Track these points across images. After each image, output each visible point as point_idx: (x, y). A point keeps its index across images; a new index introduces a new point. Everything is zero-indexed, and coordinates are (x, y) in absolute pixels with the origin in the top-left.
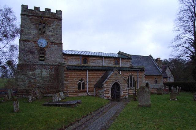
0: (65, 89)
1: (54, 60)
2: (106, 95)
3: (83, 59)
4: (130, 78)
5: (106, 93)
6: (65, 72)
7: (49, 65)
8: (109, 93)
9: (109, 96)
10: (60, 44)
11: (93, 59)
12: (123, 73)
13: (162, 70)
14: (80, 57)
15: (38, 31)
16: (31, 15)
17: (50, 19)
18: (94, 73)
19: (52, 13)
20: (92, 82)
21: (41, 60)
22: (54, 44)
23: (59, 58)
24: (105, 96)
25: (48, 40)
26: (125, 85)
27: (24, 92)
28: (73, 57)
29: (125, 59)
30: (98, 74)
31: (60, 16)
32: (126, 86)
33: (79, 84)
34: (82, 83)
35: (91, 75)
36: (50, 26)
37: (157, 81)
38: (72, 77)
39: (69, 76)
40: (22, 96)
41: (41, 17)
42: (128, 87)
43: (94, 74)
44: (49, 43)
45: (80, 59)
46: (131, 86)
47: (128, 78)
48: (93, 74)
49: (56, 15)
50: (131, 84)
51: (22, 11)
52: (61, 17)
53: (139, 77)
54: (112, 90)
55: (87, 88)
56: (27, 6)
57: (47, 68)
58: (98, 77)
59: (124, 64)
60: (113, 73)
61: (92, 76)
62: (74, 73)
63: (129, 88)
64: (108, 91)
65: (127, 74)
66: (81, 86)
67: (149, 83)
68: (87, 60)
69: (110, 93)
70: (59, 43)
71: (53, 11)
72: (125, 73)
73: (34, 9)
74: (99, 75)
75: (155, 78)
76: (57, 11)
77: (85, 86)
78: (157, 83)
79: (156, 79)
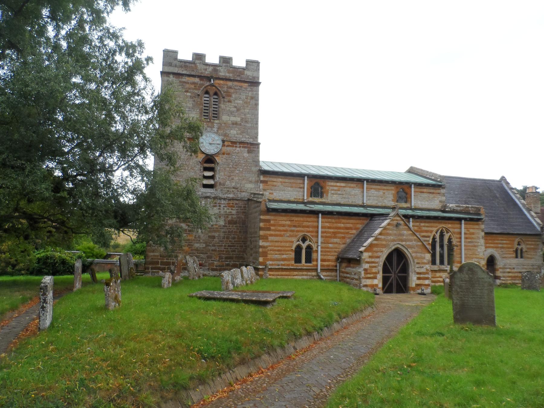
0: (261, 259)
1: (238, 186)
2: (369, 282)
3: (313, 183)
4: (438, 239)
5: (369, 276)
6: (262, 217)
7: (224, 199)
8: (375, 278)
9: (377, 285)
10: (253, 147)
11: (338, 184)
12: (418, 224)
13: (539, 221)
14: (304, 180)
15: (201, 113)
16: (184, 72)
17: (230, 84)
18: (337, 220)
19: (235, 68)
20: (330, 245)
21: (205, 186)
22: (238, 145)
23: (251, 182)
24: (366, 286)
25: (225, 135)
26: (424, 258)
27: (162, 263)
28: (287, 180)
29: (427, 185)
30: (348, 225)
31: (255, 74)
32: (425, 261)
33: (298, 250)
34: (304, 246)
35: (329, 228)
36: (230, 101)
37: (521, 250)
38: (278, 231)
39: (272, 228)
40: (158, 272)
41: (209, 78)
42: (433, 262)
43: (339, 225)
44: (226, 143)
45: (302, 186)
46: (442, 262)
47: (434, 239)
48: (335, 225)
49: (246, 72)
50: (442, 256)
51: (164, 64)
52: (258, 78)
53: (467, 236)
54: (385, 270)
55: (317, 260)
56: (176, 52)
57: (220, 206)
58: (348, 233)
59: (420, 202)
60: (389, 224)
61: (332, 230)
62: (284, 220)
63: (435, 268)
64: (374, 270)
65: (431, 229)
66: (303, 254)
67: (497, 255)
68: (322, 188)
69: (380, 276)
70: (252, 144)
71: (239, 62)
72: (424, 225)
73: (191, 60)
74: (350, 228)
75: (516, 243)
76: (249, 62)
77: (314, 256)
78: (522, 257)
79: (519, 244)
